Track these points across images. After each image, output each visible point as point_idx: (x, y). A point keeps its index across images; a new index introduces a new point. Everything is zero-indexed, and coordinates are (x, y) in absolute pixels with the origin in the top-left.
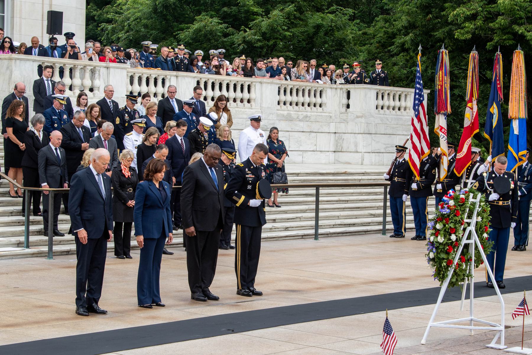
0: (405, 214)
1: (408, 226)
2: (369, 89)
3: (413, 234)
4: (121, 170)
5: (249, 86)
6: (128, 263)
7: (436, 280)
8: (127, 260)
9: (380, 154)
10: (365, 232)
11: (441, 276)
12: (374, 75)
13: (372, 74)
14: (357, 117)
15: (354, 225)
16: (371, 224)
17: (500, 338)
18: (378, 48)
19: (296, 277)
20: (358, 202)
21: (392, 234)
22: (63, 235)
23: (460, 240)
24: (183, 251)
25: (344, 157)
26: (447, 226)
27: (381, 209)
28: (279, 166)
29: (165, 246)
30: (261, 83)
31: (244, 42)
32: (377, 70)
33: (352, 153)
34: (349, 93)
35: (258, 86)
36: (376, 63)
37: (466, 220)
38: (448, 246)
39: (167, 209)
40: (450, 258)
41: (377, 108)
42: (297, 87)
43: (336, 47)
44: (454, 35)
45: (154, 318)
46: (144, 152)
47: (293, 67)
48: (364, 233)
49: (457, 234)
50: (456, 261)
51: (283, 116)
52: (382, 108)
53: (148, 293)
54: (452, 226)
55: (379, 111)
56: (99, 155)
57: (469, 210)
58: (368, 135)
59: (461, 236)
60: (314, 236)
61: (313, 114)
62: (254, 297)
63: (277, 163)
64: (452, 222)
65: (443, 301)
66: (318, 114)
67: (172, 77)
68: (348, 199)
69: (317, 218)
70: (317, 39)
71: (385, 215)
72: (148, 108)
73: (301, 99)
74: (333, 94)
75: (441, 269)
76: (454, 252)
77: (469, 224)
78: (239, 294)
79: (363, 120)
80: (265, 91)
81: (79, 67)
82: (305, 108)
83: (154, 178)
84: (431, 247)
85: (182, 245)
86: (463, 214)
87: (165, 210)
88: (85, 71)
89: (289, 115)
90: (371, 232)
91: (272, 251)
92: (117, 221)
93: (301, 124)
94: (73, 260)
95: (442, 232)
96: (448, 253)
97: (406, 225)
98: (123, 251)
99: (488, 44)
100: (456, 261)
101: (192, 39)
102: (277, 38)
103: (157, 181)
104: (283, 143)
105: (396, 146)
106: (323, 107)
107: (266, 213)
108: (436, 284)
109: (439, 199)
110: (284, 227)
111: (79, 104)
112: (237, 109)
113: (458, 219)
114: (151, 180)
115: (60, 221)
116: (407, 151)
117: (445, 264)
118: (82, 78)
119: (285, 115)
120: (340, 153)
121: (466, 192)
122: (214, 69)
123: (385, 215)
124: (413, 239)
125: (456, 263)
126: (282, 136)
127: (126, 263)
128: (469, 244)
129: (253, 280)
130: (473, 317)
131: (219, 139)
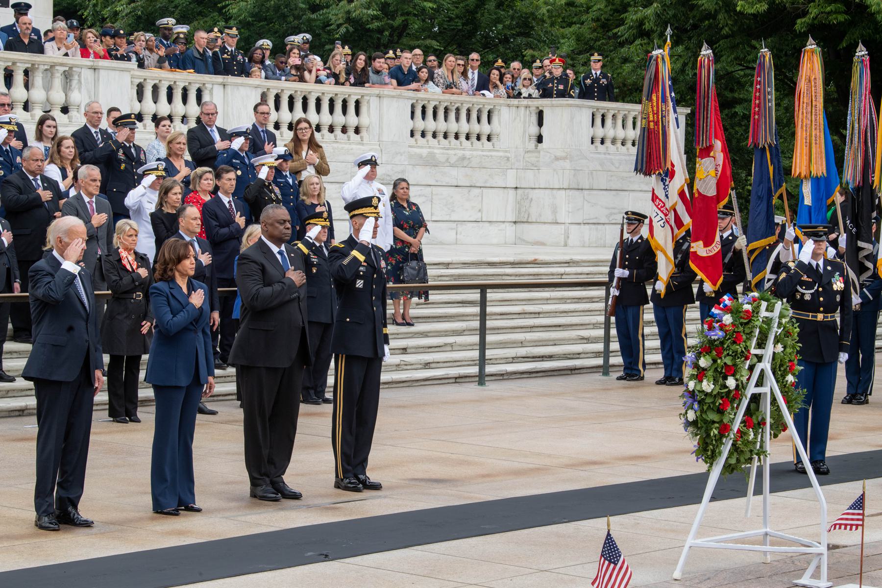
0: (643, 336)
1: (649, 358)
2: (577, 106)
3: (660, 374)
4: (120, 260)
5: (357, 103)
6: (135, 430)
7: (700, 460)
8: (131, 425)
9: (600, 227)
10: (571, 370)
11: (709, 453)
12: (588, 81)
13: (585, 78)
14: (557, 159)
15: (550, 357)
16: (582, 356)
17: (818, 567)
18: (595, 30)
19: (444, 455)
20: (558, 314)
21: (621, 374)
22: (12, 380)
23: (744, 387)
24: (236, 407)
25: (532, 232)
26: (719, 361)
27: (600, 328)
28: (413, 250)
29: (203, 399)
30: (379, 96)
31: (349, 20)
32: (594, 72)
33: (547, 226)
34: (540, 114)
35: (374, 101)
36: (592, 58)
37: (753, 351)
38: (722, 398)
39: (204, 332)
40: (725, 421)
41: (592, 143)
42: (446, 104)
43: (518, 30)
44: (736, 5)
45: (180, 533)
46: (165, 224)
47: (440, 66)
48: (569, 372)
49: (738, 377)
50: (736, 426)
51: (420, 156)
52: (602, 142)
53: (173, 488)
54: (729, 363)
55: (596, 147)
56: (65, 228)
57: (760, 332)
58: (577, 193)
59: (744, 379)
60: (477, 379)
61: (475, 153)
62: (367, 493)
63: (410, 245)
64: (728, 355)
65: (713, 499)
66: (484, 153)
67: (216, 87)
68: (541, 310)
69: (483, 346)
70: (483, 15)
71: (607, 339)
72: (170, 142)
73: (453, 126)
74: (512, 120)
75: (708, 441)
76: (733, 408)
77: (760, 358)
78: (339, 488)
79: (567, 164)
80: (386, 110)
81: (42, 67)
82: (461, 143)
83: (177, 274)
84: (690, 401)
85: (235, 397)
86: (749, 339)
87: (200, 335)
88: (52, 74)
89: (432, 155)
90: (581, 371)
91: (399, 407)
92: (115, 353)
93: (454, 172)
94: (31, 426)
95: (710, 373)
96: (720, 411)
97: (646, 357)
98: (123, 409)
99: (799, 21)
100: (736, 426)
101: (253, 15)
102: (408, 14)
103: (183, 275)
104: (418, 208)
105: (627, 213)
106: (494, 140)
107: (390, 337)
108: (701, 467)
109: (705, 313)
110: (423, 362)
111: (40, 136)
112: (335, 145)
113: (739, 348)
114: (172, 279)
115: (7, 353)
116: (647, 221)
117: (716, 432)
118: (48, 87)
119: (424, 155)
120: (526, 226)
121: (754, 300)
122: (293, 72)
123: (607, 339)
124: (659, 383)
125: (735, 430)
126: (415, 196)
127: (130, 431)
128: (760, 394)
129: (365, 460)
130: (768, 530)
131: (303, 201)
